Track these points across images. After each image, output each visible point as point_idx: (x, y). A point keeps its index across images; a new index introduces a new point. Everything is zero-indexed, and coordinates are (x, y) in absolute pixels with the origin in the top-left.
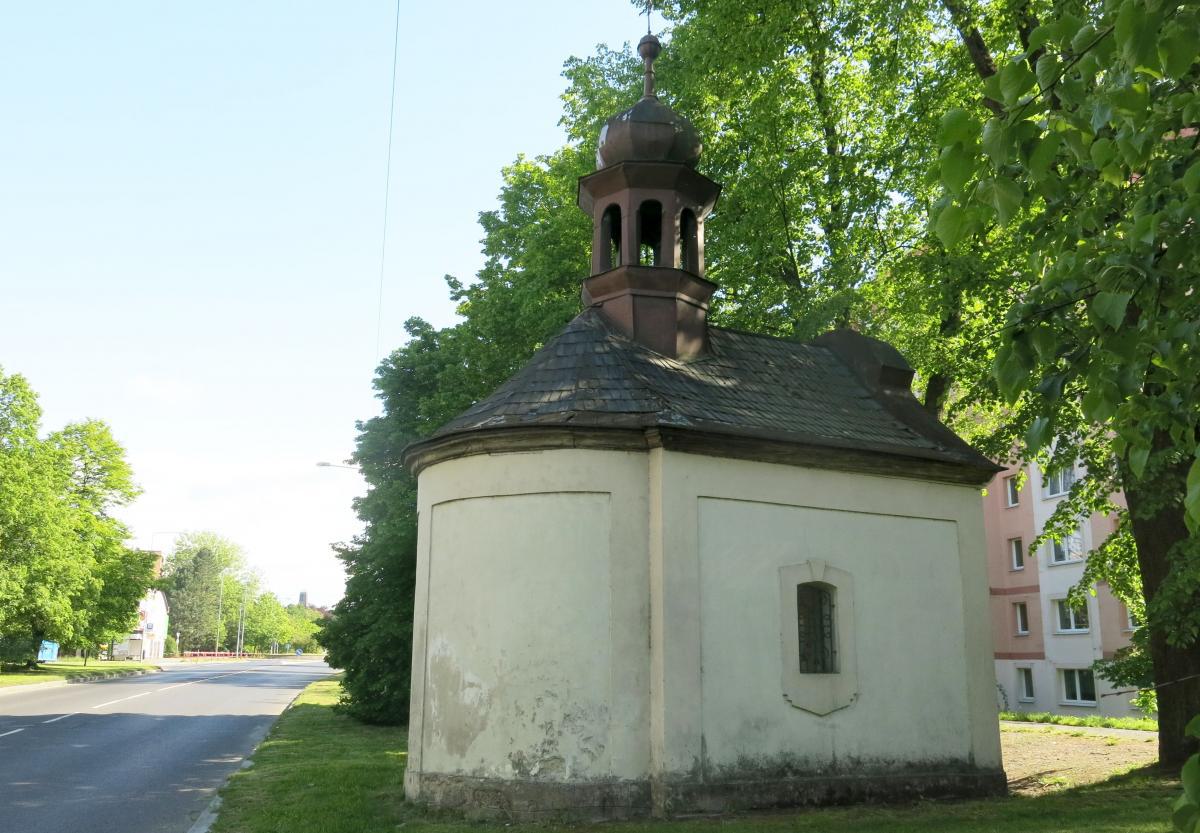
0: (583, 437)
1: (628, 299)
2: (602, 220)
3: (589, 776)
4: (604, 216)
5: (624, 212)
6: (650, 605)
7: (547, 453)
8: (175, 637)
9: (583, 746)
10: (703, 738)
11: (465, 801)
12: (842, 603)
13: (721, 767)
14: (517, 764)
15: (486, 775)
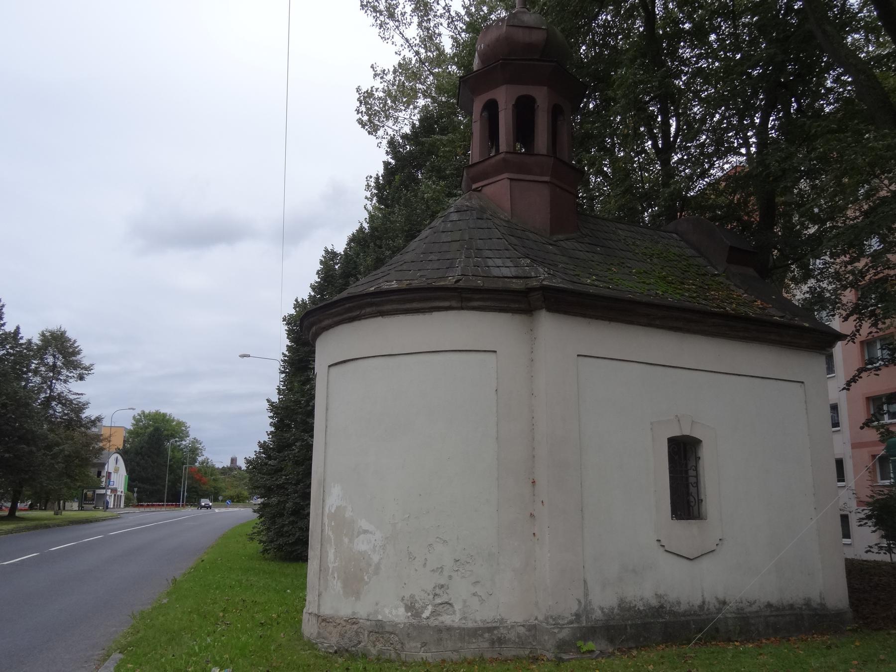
0: (470, 300)
1: (507, 183)
2: (481, 115)
3: (478, 619)
4: (482, 112)
5: (501, 106)
6: (324, 480)
7: (436, 315)
8: (133, 492)
10: (585, 582)
11: (360, 642)
13: (602, 609)
14: (410, 607)
15: (380, 617)
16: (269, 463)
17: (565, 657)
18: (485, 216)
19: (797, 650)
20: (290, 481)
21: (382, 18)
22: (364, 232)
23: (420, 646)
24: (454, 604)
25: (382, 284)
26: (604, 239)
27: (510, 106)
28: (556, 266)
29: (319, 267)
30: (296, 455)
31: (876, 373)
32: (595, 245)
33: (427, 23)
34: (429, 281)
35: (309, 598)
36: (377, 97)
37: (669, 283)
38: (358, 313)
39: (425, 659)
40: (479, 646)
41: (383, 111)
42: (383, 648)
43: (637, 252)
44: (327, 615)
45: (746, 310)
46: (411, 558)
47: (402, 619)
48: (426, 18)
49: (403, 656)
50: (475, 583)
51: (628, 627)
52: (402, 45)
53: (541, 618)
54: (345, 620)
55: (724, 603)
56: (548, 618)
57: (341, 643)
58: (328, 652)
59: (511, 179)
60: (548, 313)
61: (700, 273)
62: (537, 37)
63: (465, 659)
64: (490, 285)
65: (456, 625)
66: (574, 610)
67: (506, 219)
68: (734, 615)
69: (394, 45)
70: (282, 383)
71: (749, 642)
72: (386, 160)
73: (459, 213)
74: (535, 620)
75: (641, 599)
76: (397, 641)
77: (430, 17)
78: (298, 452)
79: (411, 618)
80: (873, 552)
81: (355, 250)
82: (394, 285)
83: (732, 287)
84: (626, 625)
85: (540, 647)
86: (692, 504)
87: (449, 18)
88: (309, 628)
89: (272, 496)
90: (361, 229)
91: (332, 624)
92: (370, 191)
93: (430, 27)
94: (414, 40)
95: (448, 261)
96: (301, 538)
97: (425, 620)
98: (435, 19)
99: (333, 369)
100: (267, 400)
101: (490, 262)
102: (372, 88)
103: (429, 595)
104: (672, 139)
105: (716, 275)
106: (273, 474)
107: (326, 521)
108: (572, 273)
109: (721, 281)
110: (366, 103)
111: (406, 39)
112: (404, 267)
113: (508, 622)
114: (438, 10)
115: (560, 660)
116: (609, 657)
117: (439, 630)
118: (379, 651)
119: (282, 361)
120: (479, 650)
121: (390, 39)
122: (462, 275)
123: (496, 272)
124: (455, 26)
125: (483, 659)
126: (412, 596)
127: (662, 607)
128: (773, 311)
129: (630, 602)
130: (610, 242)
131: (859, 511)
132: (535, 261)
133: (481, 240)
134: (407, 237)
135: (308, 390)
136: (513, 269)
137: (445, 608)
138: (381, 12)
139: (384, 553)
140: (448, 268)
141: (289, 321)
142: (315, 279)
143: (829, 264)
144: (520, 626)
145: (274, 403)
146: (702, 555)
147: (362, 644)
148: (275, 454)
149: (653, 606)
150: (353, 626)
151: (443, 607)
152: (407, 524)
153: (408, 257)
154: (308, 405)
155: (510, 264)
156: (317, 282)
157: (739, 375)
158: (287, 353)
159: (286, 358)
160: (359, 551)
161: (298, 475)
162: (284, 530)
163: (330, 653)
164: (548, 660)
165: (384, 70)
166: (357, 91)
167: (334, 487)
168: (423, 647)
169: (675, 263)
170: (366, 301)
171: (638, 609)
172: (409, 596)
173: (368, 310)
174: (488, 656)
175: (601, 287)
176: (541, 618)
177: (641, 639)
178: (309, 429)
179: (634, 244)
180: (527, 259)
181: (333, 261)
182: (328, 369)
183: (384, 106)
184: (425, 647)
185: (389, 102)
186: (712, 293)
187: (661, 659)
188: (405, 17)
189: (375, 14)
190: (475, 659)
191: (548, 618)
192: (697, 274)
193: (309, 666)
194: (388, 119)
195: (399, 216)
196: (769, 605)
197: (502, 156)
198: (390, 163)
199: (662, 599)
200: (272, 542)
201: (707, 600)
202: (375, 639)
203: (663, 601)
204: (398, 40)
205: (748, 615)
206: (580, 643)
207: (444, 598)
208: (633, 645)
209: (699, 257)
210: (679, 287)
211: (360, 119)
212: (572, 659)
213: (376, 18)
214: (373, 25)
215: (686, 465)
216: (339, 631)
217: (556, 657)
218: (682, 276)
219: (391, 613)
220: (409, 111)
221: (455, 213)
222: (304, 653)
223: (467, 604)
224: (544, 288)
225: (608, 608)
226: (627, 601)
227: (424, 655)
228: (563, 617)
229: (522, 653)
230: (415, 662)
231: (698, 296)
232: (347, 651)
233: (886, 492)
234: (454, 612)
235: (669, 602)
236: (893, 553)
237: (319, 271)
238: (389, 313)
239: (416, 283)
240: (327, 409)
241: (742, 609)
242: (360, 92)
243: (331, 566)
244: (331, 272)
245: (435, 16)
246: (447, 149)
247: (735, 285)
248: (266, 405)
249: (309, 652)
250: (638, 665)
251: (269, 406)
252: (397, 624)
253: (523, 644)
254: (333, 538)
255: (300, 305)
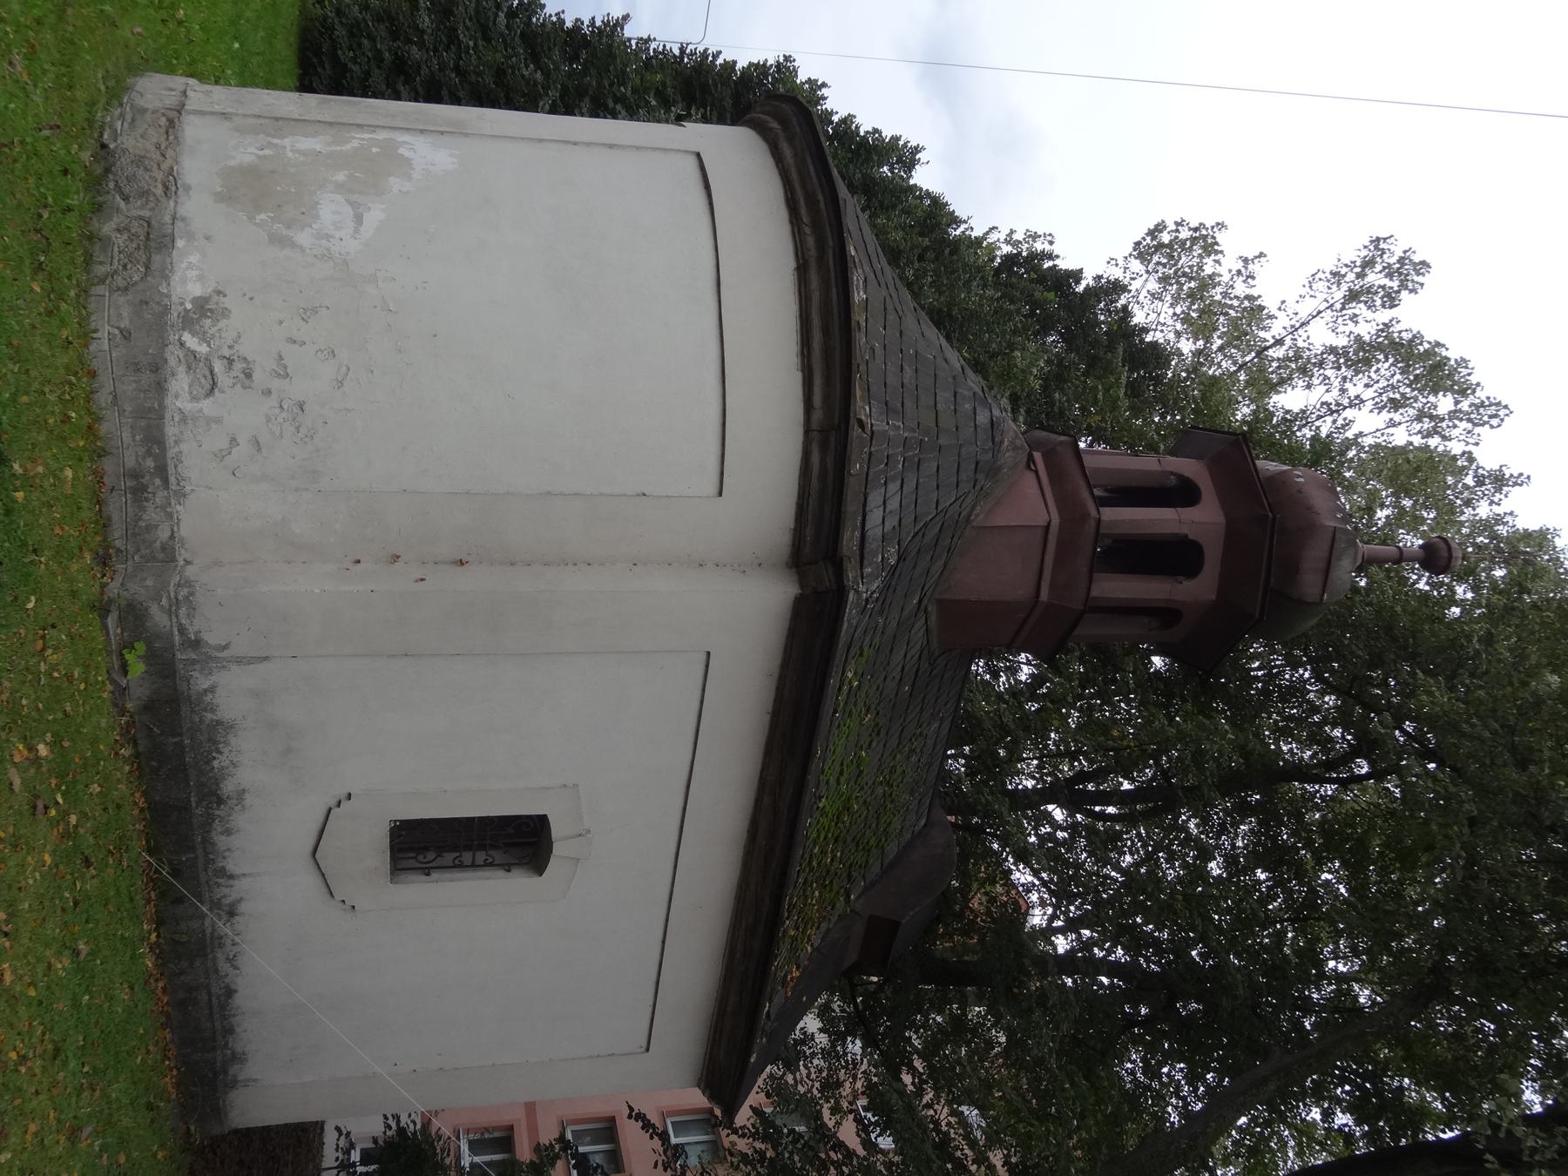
0: (824, 447)
3: (184, 447)
6: (466, 135)
7: (796, 379)
9: (243, 439)
10: (266, 658)
11: (126, 199)
12: (519, 883)
13: (212, 689)
14: (203, 307)
15: (180, 243)
16: (500, 13)
17: (111, 621)
18: (980, 476)
19: (143, 1050)
20: (463, 55)
21: (1351, 276)
22: (949, 225)
23: (122, 326)
24: (211, 399)
25: (860, 271)
26: (925, 697)
27: (1185, 530)
28: (881, 612)
29: (888, 134)
30: (517, 72)
31: (660, 1163)
32: (914, 683)
33: (1333, 363)
34: (863, 368)
35: (219, 92)
36: (1204, 261)
37: (838, 818)
38: (805, 220)
39: (95, 335)
40: (128, 448)
41: (1176, 272)
42: (116, 249)
43: (898, 756)
44: (183, 130)
45: (784, 953)
46: (305, 313)
47: (179, 290)
48: (1342, 361)
49: (100, 290)
50: (258, 442)
51: (176, 739)
52: (1297, 314)
53: (190, 571)
54: (172, 168)
55: (232, 913)
56: (190, 586)
57: (123, 159)
58: (104, 130)
59: (1047, 527)
60: (792, 599)
61: (853, 869)
62: (1309, 584)
63: (99, 420)
64: (853, 485)
65: (169, 401)
66: (205, 636)
67: (972, 518)
68: (208, 931)
69: (1299, 298)
70: (661, 49)
71: (158, 957)
72: (1084, 275)
73: (989, 426)
74: (185, 560)
75: (234, 764)
76: (131, 278)
77: (1343, 369)
78: (523, 76)
79: (180, 308)
80: (338, 1140)
81: (916, 207)
82: (859, 296)
83: (824, 926)
84: (180, 735)
85: (130, 569)
86: (421, 857)
87: (1338, 404)
88: (154, 90)
89: (433, 16)
90: (956, 221)
91: (163, 139)
92: (1024, 239)
93: (1325, 369)
94: (1305, 337)
95: (900, 405)
96: (348, 75)
97: (177, 337)
98: (1339, 379)
99: (692, 162)
100: (628, 15)
101: (894, 487)
102: (1222, 252)
103: (230, 347)
104: (1097, 809)
105: (848, 896)
106: (478, 21)
107: (382, 135)
108: (867, 641)
109: (838, 905)
110: (1194, 240)
111: (1308, 322)
112: (892, 317)
113: (178, 506)
114: (1355, 385)
115: (103, 609)
116: (116, 705)
117: (157, 367)
118: (109, 238)
119: (706, 50)
120: (118, 448)
121: (1309, 290)
122: (872, 432)
123: (875, 498)
124: (1322, 417)
125: (99, 456)
126: (226, 313)
127: (220, 801)
128: (778, 999)
129: (227, 743)
130: (918, 709)
131: (413, 1115)
132: (893, 574)
133: (935, 469)
134: (940, 311)
135: (648, 102)
136: (879, 532)
137: (203, 380)
138: (1361, 276)
139: (315, 256)
140: (886, 404)
141: (785, 69)
142: (865, 124)
143: (853, 1069)
144: (172, 530)
145: (622, 29)
146: (323, 875)
147: (122, 204)
148: (518, 27)
149: (221, 786)
150: (160, 186)
151: (205, 377)
152: (375, 307)
153: (910, 321)
154: (617, 100)
155: (888, 526)
156: (857, 128)
157: (663, 942)
158: (720, 61)
159: (710, 58)
160: (318, 203)
161: (475, 73)
162: (362, 39)
163: (101, 135)
164: (103, 586)
165: (1253, 278)
166: (1218, 224)
167: (451, 155)
168: (121, 332)
169: (874, 825)
170: (829, 235)
171: (214, 758)
172: (226, 305)
173: (811, 241)
174: (108, 465)
175: (837, 699)
176: (190, 571)
177: (154, 763)
178: (566, 106)
179: (912, 751)
180: (896, 558)
181: (897, 163)
182: (693, 152)
183: (1185, 274)
184: (119, 336)
185: (1193, 284)
186: (817, 893)
187: (114, 806)
188: (1348, 322)
189: (1358, 264)
190: (100, 439)
191: (190, 586)
192: (851, 864)
193: (71, 87)
194: (1160, 280)
195: (975, 297)
196: (230, 992)
197: (1093, 512)
198: (1078, 282)
199: (234, 801)
200: (339, 12)
201: (236, 882)
202: (133, 231)
203: (231, 803)
204: (1306, 309)
205: (210, 956)
206: (141, 647)
207: (223, 379)
208: (141, 749)
209: (882, 865)
210: (830, 835)
211: (1165, 227)
212: (108, 634)
213: (1351, 266)
214: (1339, 260)
215: (494, 847)
216: (148, 155)
217: (110, 601)
218: (849, 839)
219: (190, 266)
220: (1170, 322)
221: (988, 420)
222: (100, 76)
223: (213, 426)
224: (841, 592)
225: (214, 701)
226: (230, 737)
227: (104, 333)
228: (194, 617)
229: (117, 535)
230: (89, 314)
231: (812, 870)
232: (107, 170)
233: (447, 1161)
234: (195, 399)
235: (229, 815)
236: (339, 1172)
237: (880, 133)
238: (803, 286)
239: (860, 339)
240: (611, 146)
241: (221, 946)
242: (1215, 230)
243: (287, 142)
244: (875, 158)
245: (1344, 379)
246: (1100, 396)
247: (828, 930)
248: (617, 14)
249: (103, 88)
250: (99, 764)
251: (615, 18)
252: (167, 278)
253: (135, 535)
254: (343, 148)
255: (815, 91)
